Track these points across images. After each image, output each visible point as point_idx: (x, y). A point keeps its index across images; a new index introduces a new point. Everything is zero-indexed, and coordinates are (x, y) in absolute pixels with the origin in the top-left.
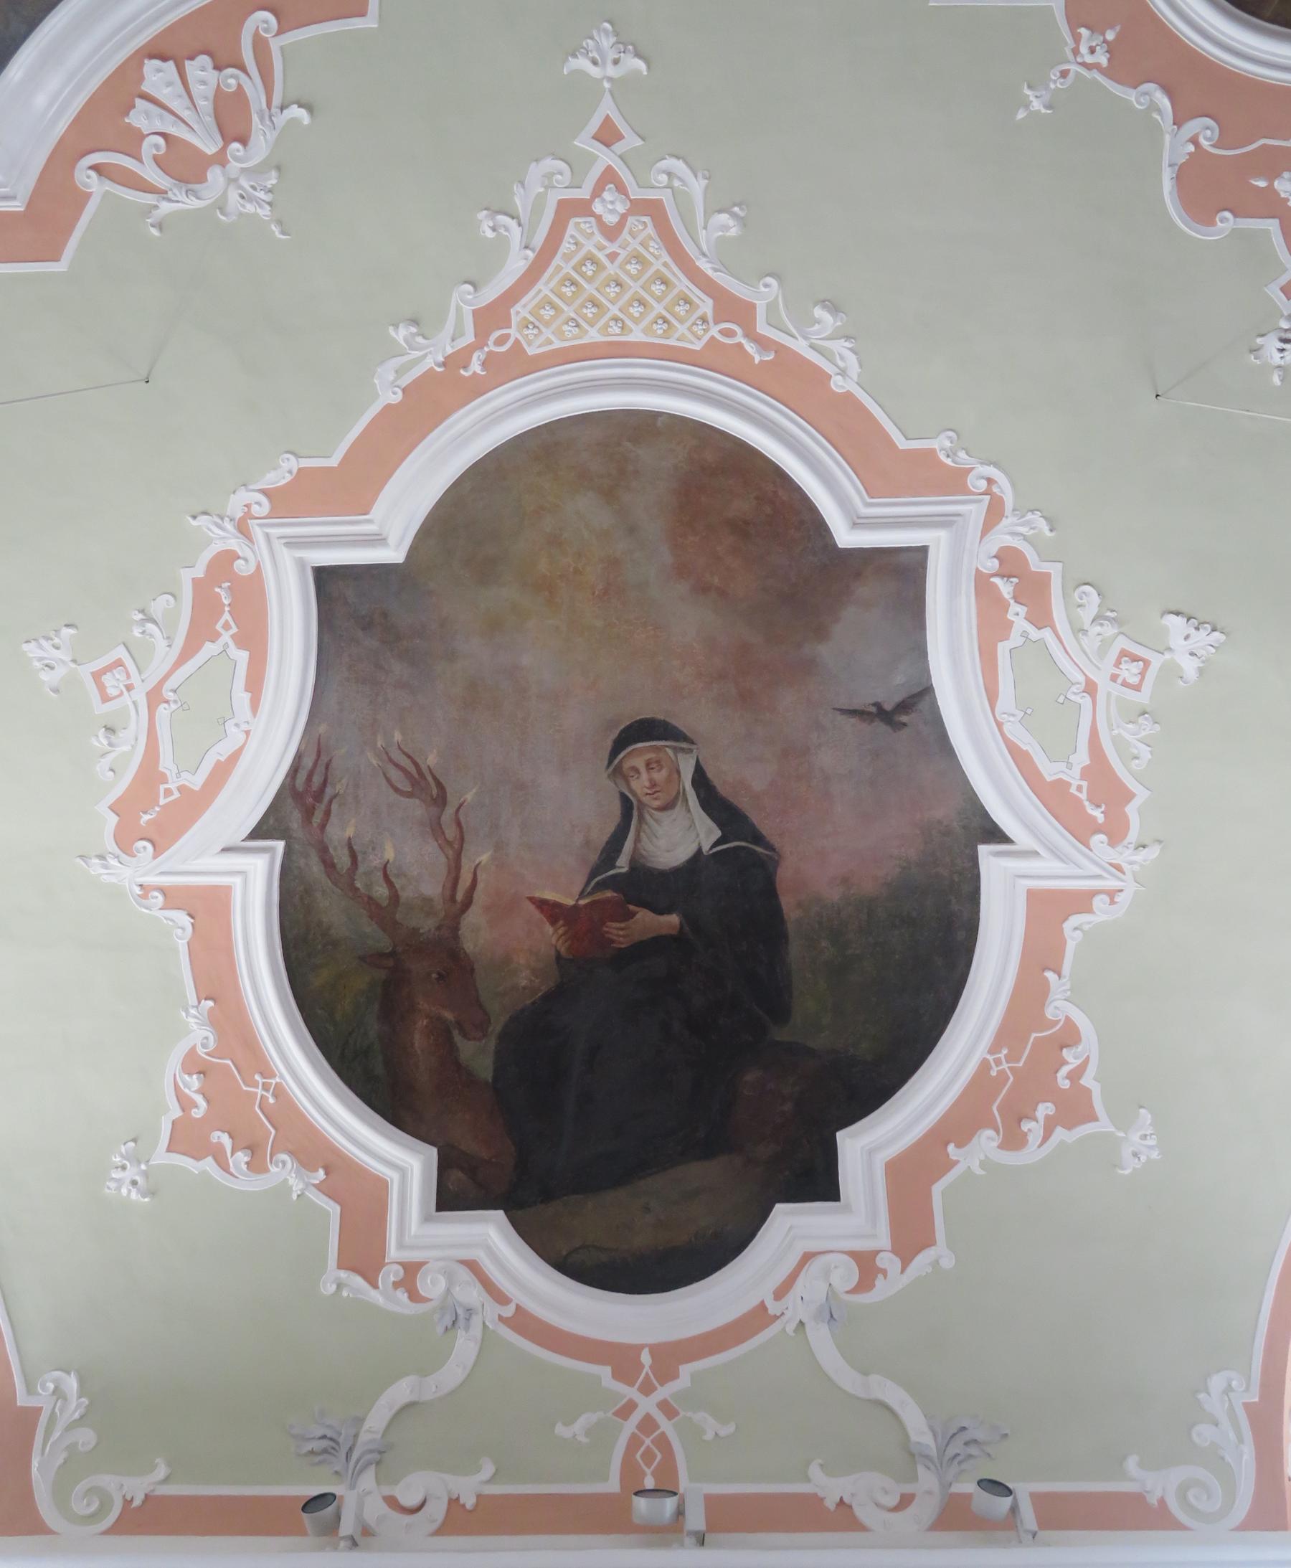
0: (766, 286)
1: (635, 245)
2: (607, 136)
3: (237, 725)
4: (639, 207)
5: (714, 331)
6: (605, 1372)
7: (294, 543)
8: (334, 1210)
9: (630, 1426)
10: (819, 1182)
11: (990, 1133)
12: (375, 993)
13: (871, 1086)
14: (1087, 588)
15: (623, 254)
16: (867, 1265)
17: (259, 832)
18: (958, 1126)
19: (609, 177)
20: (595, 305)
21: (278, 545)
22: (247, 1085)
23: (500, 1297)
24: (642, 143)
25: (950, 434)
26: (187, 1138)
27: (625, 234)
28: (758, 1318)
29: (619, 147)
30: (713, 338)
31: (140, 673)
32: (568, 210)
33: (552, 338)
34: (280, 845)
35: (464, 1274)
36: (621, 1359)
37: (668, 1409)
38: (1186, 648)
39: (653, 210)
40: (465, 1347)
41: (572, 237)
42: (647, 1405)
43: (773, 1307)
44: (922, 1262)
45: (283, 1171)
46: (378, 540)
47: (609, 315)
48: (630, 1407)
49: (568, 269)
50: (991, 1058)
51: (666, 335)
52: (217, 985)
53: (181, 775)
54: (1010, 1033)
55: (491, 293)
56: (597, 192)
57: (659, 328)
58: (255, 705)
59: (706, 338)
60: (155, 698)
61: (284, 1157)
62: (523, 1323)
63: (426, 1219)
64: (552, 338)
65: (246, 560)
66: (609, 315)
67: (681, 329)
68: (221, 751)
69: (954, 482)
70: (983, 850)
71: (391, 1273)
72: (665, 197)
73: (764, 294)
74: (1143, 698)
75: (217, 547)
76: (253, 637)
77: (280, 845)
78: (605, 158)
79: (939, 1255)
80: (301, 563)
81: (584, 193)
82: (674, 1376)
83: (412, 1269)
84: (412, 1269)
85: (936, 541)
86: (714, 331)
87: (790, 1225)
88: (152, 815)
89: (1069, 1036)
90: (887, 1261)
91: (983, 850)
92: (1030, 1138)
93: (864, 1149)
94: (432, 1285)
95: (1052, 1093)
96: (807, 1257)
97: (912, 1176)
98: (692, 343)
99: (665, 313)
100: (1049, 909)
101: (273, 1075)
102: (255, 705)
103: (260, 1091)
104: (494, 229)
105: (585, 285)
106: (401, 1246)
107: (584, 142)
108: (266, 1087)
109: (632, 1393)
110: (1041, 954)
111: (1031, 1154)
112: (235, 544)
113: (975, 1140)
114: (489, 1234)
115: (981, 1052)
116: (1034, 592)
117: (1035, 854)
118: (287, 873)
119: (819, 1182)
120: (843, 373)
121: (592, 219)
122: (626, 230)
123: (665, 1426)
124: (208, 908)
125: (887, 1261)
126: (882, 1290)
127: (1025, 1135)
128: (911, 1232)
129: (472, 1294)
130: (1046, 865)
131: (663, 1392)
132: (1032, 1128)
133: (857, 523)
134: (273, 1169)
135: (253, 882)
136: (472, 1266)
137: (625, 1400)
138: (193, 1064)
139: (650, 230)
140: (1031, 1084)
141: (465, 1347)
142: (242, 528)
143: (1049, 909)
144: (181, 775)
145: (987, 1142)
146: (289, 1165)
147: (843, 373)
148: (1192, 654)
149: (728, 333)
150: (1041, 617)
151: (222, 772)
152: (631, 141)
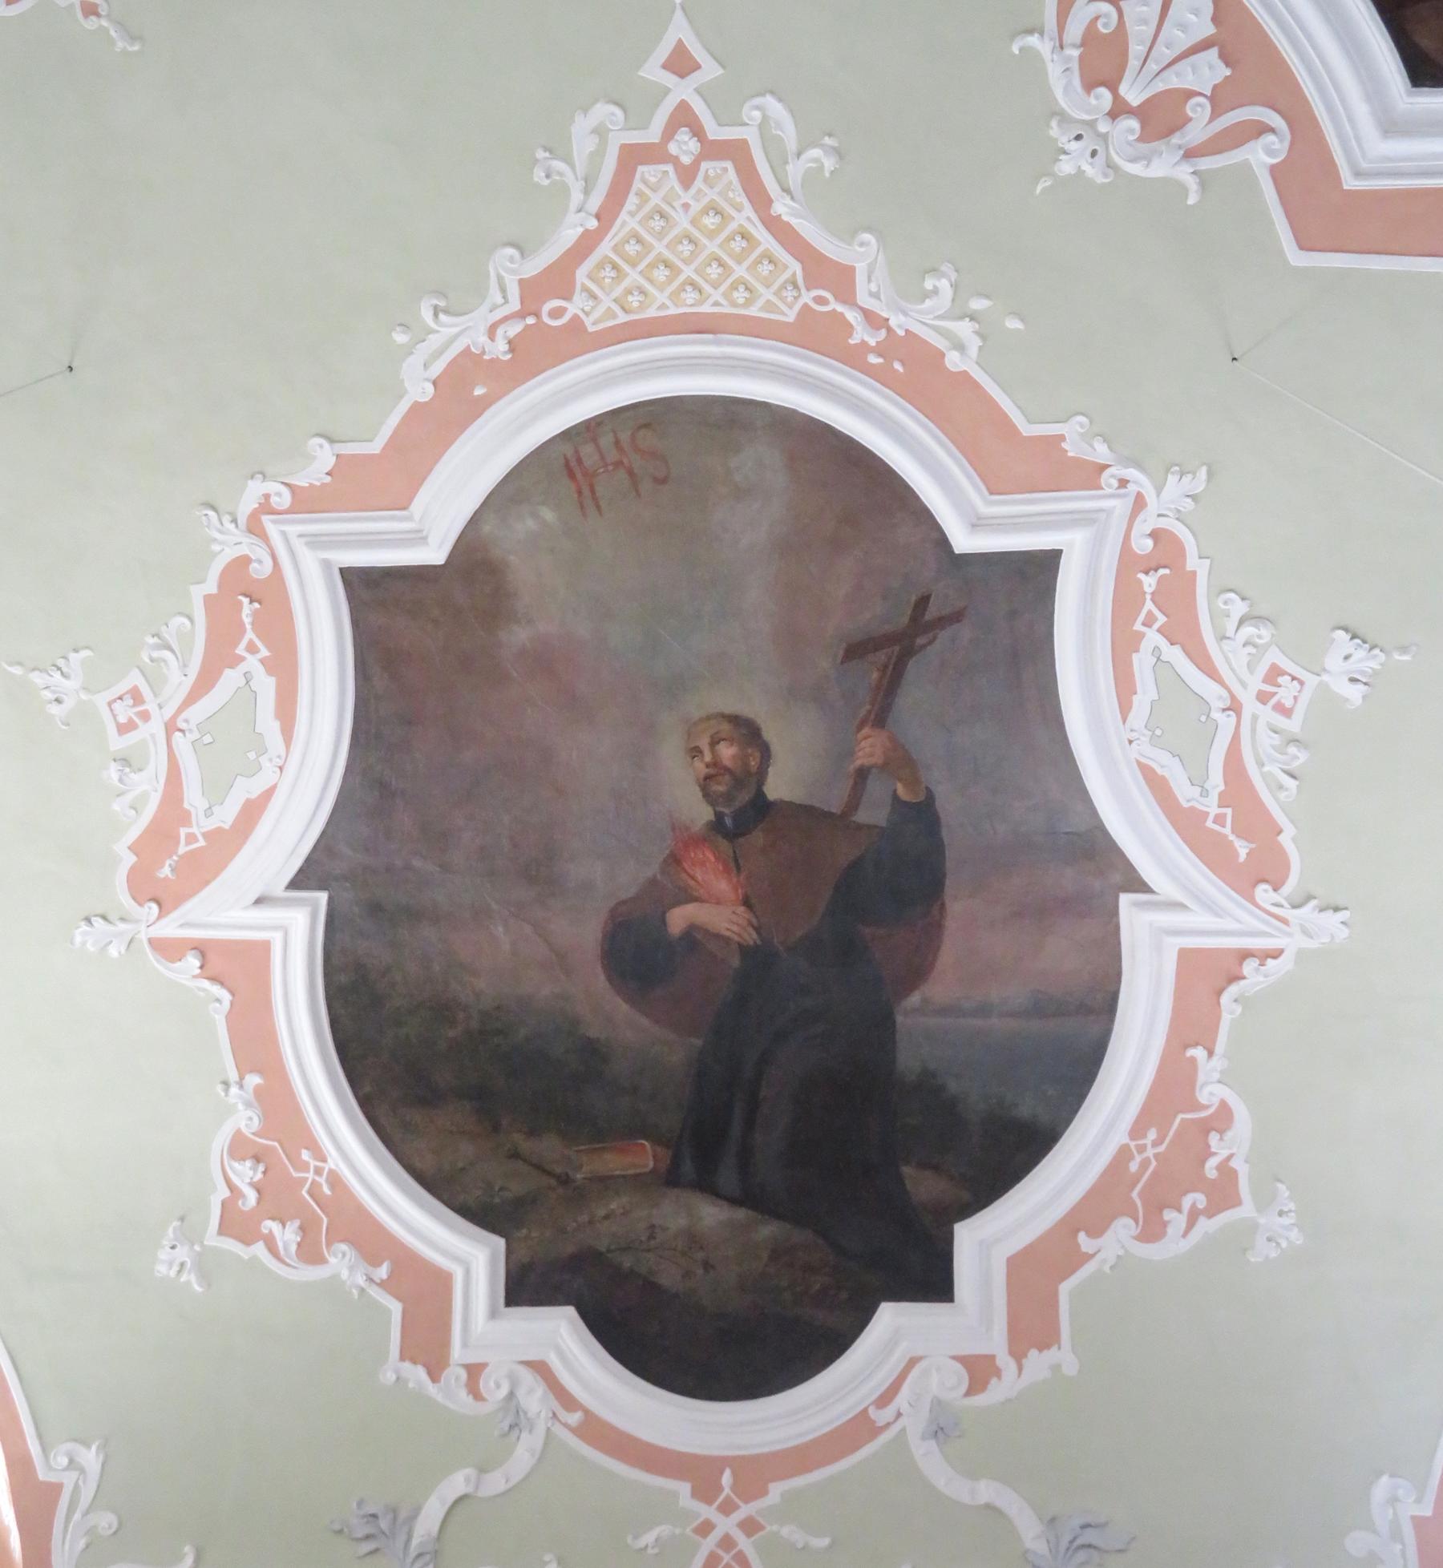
0: (862, 244)
1: (712, 195)
2: (681, 64)
3: (271, 760)
4: (713, 150)
5: (807, 297)
6: (684, 1488)
7: (315, 542)
8: (395, 1308)
9: (710, 1543)
10: (933, 1281)
11: (1131, 1222)
12: (434, 1066)
14: (1232, 595)
15: (696, 207)
17: (299, 882)
18: (1093, 1212)
19: (683, 118)
20: (720, 265)
21: (299, 546)
22: (297, 1170)
23: (567, 1400)
24: (721, 71)
25: (1081, 418)
26: (236, 1224)
27: (699, 183)
28: (858, 1430)
29: (696, 79)
30: (806, 305)
31: (156, 695)
32: (633, 157)
33: (668, 303)
34: (323, 897)
35: (527, 1377)
36: (701, 1473)
37: (750, 1527)
38: (1342, 667)
39: (736, 153)
40: (523, 1455)
41: (639, 194)
42: (726, 1525)
43: (881, 1416)
44: (1038, 1363)
45: (342, 1263)
46: (419, 538)
47: (682, 278)
48: (705, 1528)
49: (633, 224)
50: (1132, 1144)
51: (748, 303)
52: (254, 1041)
53: (209, 814)
54: (1153, 1112)
55: (534, 267)
56: (669, 133)
57: (690, 296)
58: (288, 733)
59: (797, 307)
60: (171, 728)
61: (344, 1247)
62: (596, 1431)
63: (493, 1314)
64: (668, 303)
65: (260, 562)
66: (682, 278)
67: (717, 295)
68: (246, 789)
69: (1089, 475)
70: (1125, 899)
71: (455, 1374)
72: (751, 135)
73: (862, 254)
74: (1294, 725)
75: (230, 554)
76: (284, 666)
77: (323, 897)
78: (683, 90)
79: (1064, 1357)
80: (326, 565)
81: (652, 134)
82: (764, 1492)
83: (474, 1371)
84: (474, 1371)
85: (1073, 544)
86: (807, 297)
87: (893, 1323)
88: (171, 863)
89: (1223, 1118)
90: (1005, 1361)
91: (1125, 899)
92: (1170, 1230)
93: (984, 1243)
94: (495, 1388)
95: (1197, 1182)
96: (913, 1362)
97: (1037, 1273)
98: (784, 314)
99: (695, 277)
100: (1207, 975)
101: (324, 1160)
102: (288, 733)
103: (311, 1176)
104: (548, 176)
105: (705, 241)
106: (465, 1345)
107: (653, 71)
108: (318, 1171)
109: (708, 1512)
110: (1192, 1024)
111: (1174, 1245)
112: (248, 546)
113: (1113, 1226)
114: (559, 1333)
115: (1120, 1137)
116: (1178, 602)
117: (1181, 906)
118: (333, 922)
119: (933, 1281)
120: (960, 347)
121: (669, 168)
122: (701, 175)
123: (744, 1543)
124: (238, 966)
125: (1005, 1361)
126: (996, 1393)
127: (1165, 1224)
128: (1031, 1326)
129: (535, 1399)
130: (1199, 919)
131: (745, 1511)
132: (1176, 1220)
133: (977, 524)
134: (332, 1260)
135: (295, 936)
136: (541, 1369)
137: (701, 1520)
138: (239, 1148)
139: (732, 175)
140: (1177, 1171)
141: (523, 1455)
142: (254, 528)
143: (1207, 975)
144: (209, 814)
145: (1123, 1229)
146: (347, 1258)
147: (960, 347)
148: (1353, 680)
149: (820, 300)
150: (1183, 632)
151: (252, 811)
152: (710, 70)
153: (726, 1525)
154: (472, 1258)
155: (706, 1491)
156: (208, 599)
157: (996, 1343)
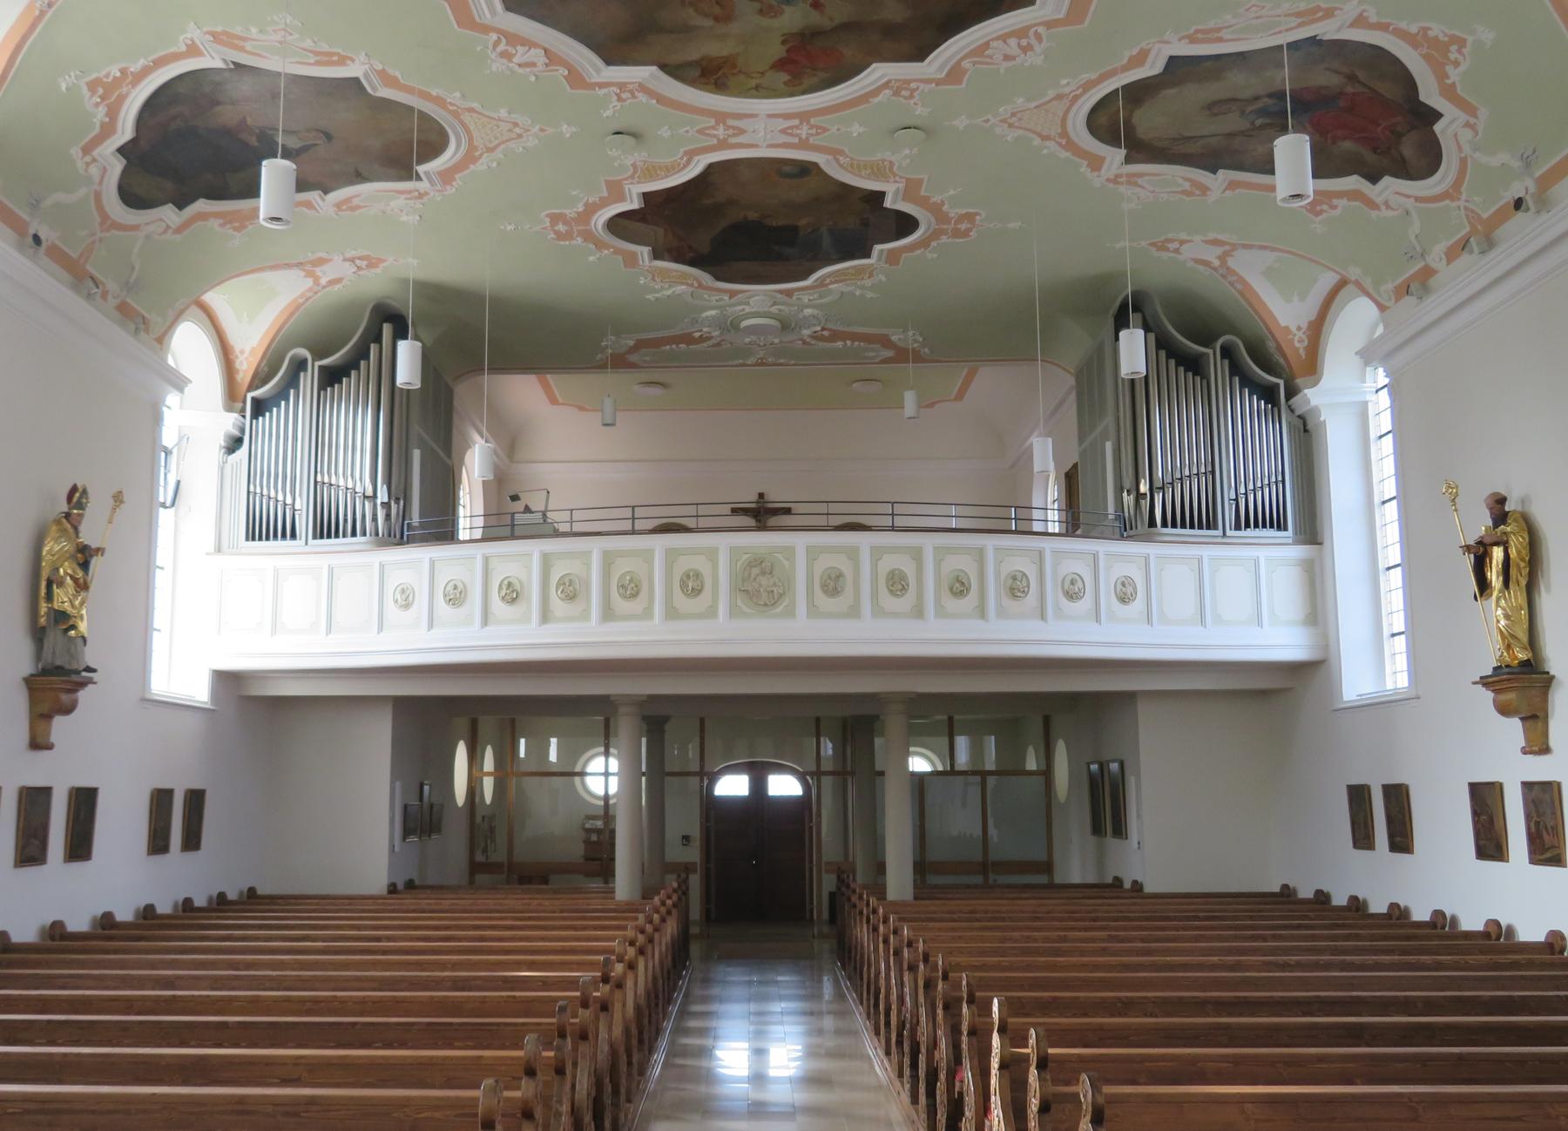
16: (1467, 125)
90: (1472, 120)
119: (1437, 116)
125: (1472, 120)
126: (1480, 128)
140: (1437, 52)
145: (1450, 69)
153: (1462, 203)
154: (1353, 182)
155: (1453, 200)
157: (1463, 117)
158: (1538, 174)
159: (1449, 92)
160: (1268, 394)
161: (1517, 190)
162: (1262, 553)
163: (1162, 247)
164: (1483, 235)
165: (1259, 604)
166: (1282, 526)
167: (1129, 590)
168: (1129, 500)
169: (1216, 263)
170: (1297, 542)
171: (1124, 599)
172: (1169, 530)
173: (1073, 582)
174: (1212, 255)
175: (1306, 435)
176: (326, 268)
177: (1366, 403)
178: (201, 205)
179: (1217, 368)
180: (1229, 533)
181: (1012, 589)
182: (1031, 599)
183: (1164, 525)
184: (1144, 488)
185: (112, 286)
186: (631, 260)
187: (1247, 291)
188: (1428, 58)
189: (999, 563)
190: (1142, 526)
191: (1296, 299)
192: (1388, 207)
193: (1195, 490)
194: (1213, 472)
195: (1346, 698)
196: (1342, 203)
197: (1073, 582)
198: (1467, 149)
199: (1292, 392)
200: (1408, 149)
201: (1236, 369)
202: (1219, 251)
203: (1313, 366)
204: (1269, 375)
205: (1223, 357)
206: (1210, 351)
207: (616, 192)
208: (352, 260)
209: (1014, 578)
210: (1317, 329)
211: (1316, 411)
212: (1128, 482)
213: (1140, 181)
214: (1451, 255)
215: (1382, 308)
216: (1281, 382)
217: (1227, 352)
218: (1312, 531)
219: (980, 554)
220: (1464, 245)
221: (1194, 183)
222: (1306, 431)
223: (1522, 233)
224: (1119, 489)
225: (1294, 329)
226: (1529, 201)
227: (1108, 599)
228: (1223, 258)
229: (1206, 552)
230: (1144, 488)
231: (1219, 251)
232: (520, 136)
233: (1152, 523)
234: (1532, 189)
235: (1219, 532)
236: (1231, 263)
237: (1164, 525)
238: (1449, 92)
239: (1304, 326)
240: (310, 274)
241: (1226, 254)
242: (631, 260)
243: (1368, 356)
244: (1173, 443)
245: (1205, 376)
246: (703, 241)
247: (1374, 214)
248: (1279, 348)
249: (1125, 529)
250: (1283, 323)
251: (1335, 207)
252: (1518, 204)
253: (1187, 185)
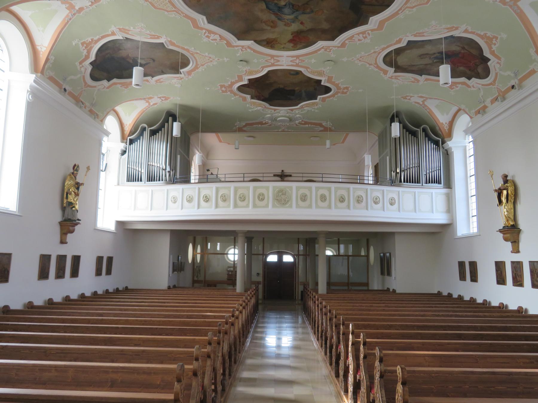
13: (481, 50)
90: (499, 62)
119: (489, 60)
125: (499, 62)
140: (489, 41)
145: (493, 46)
156: (321, 81)
157: (497, 60)
158: (519, 78)
159: (493, 53)
160: (436, 143)
161: (512, 83)
162: (434, 191)
163: (405, 98)
164: (502, 96)
165: (419, 233)
166: (439, 183)
167: (393, 201)
168: (393, 174)
169: (421, 103)
170: (444, 188)
171: (391, 204)
172: (406, 183)
173: (376, 199)
174: (420, 101)
175: (447, 156)
176: (152, 100)
177: (466, 146)
178: (115, 80)
179: (421, 135)
180: (424, 185)
181: (358, 200)
182: (364, 204)
183: (404, 182)
184: (398, 171)
185: (87, 104)
186: (244, 99)
187: (430, 112)
188: (486, 42)
189: (354, 192)
190: (398, 182)
191: (445, 114)
192: (473, 86)
193: (414, 171)
194: (419, 166)
195: (458, 235)
196: (460, 86)
197: (376, 199)
198: (498, 70)
199: (443, 142)
200: (480, 70)
201: (427, 135)
202: (422, 99)
203: (450, 135)
204: (437, 137)
205: (423, 131)
206: (419, 130)
207: (240, 78)
208: (160, 98)
209: (359, 197)
210: (451, 124)
211: (451, 148)
212: (393, 169)
213: (399, 78)
214: (492, 102)
215: (471, 118)
216: (440, 139)
217: (424, 130)
218: (449, 185)
219: (348, 190)
220: (496, 99)
221: (415, 79)
222: (447, 154)
223: (514, 96)
224: (391, 171)
225: (444, 123)
226: (516, 86)
227: (387, 204)
228: (423, 102)
229: (417, 190)
230: (398, 171)
231: (422, 99)
232: (211, 61)
233: (401, 181)
234: (517, 82)
235: (421, 184)
236: (426, 103)
237: (404, 182)
238: (493, 53)
239: (448, 122)
240: (147, 102)
241: (424, 100)
242: (244, 99)
243: (467, 132)
244: (407, 158)
245: (417, 137)
246: (266, 94)
247: (469, 89)
248: (440, 129)
249: (392, 183)
250: (441, 121)
251: (457, 87)
252: (513, 87)
253: (413, 80)
